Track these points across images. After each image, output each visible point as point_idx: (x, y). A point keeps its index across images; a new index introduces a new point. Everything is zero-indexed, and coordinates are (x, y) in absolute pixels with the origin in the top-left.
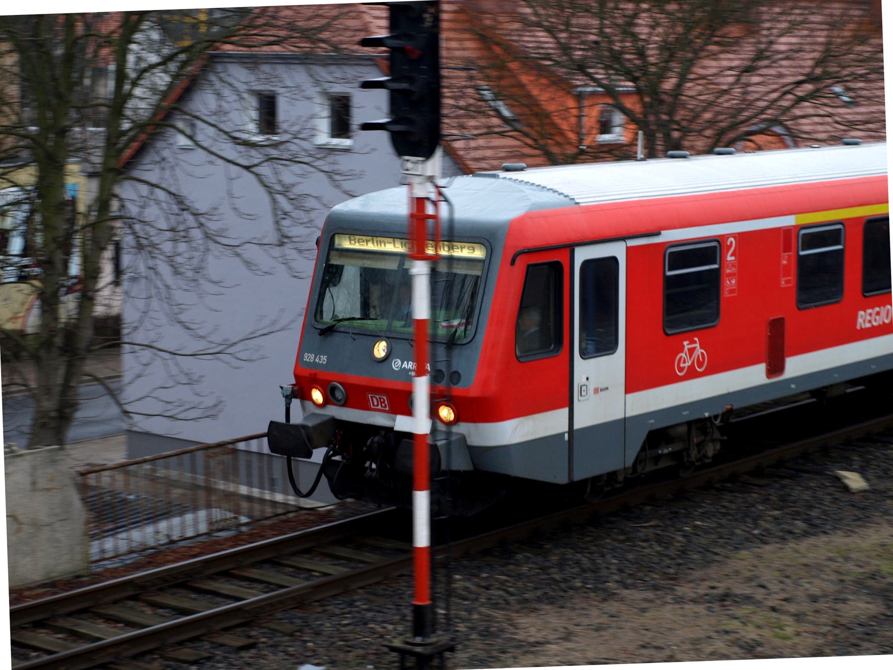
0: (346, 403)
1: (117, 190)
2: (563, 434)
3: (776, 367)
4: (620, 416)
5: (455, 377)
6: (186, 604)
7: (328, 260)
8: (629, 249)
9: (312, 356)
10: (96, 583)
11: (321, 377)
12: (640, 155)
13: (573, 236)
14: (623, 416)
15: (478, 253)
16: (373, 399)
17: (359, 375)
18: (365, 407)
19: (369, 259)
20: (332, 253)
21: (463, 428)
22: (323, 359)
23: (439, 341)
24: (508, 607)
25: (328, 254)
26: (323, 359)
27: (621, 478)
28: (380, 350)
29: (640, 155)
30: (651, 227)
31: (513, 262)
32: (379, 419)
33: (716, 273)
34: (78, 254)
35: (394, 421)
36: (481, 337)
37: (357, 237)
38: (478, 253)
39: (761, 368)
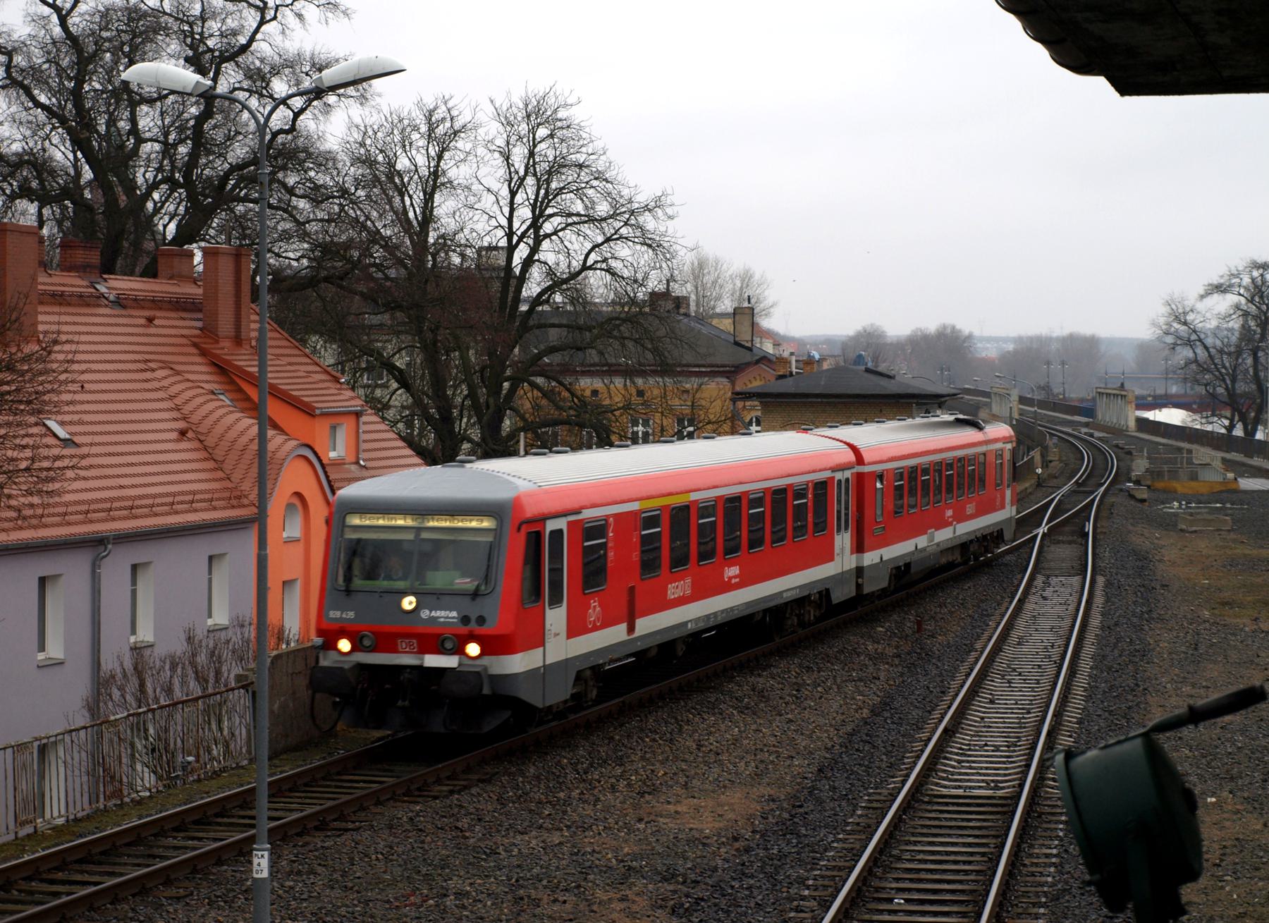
0: (374, 649)
2: (539, 668)
3: (631, 629)
4: (564, 657)
5: (481, 620)
8: (569, 523)
12: (522, 452)
13: (583, 504)
14: (541, 664)
15: (486, 523)
16: (402, 644)
18: (394, 650)
19: (376, 532)
20: (346, 529)
21: (487, 660)
22: (351, 615)
25: (342, 531)
26: (351, 615)
27: (555, 710)
28: (408, 603)
29: (522, 452)
30: (576, 506)
31: (519, 530)
32: (407, 660)
33: (604, 546)
34: (1182, 392)
35: (423, 659)
36: (499, 589)
37: (369, 515)
38: (486, 523)
39: (623, 627)
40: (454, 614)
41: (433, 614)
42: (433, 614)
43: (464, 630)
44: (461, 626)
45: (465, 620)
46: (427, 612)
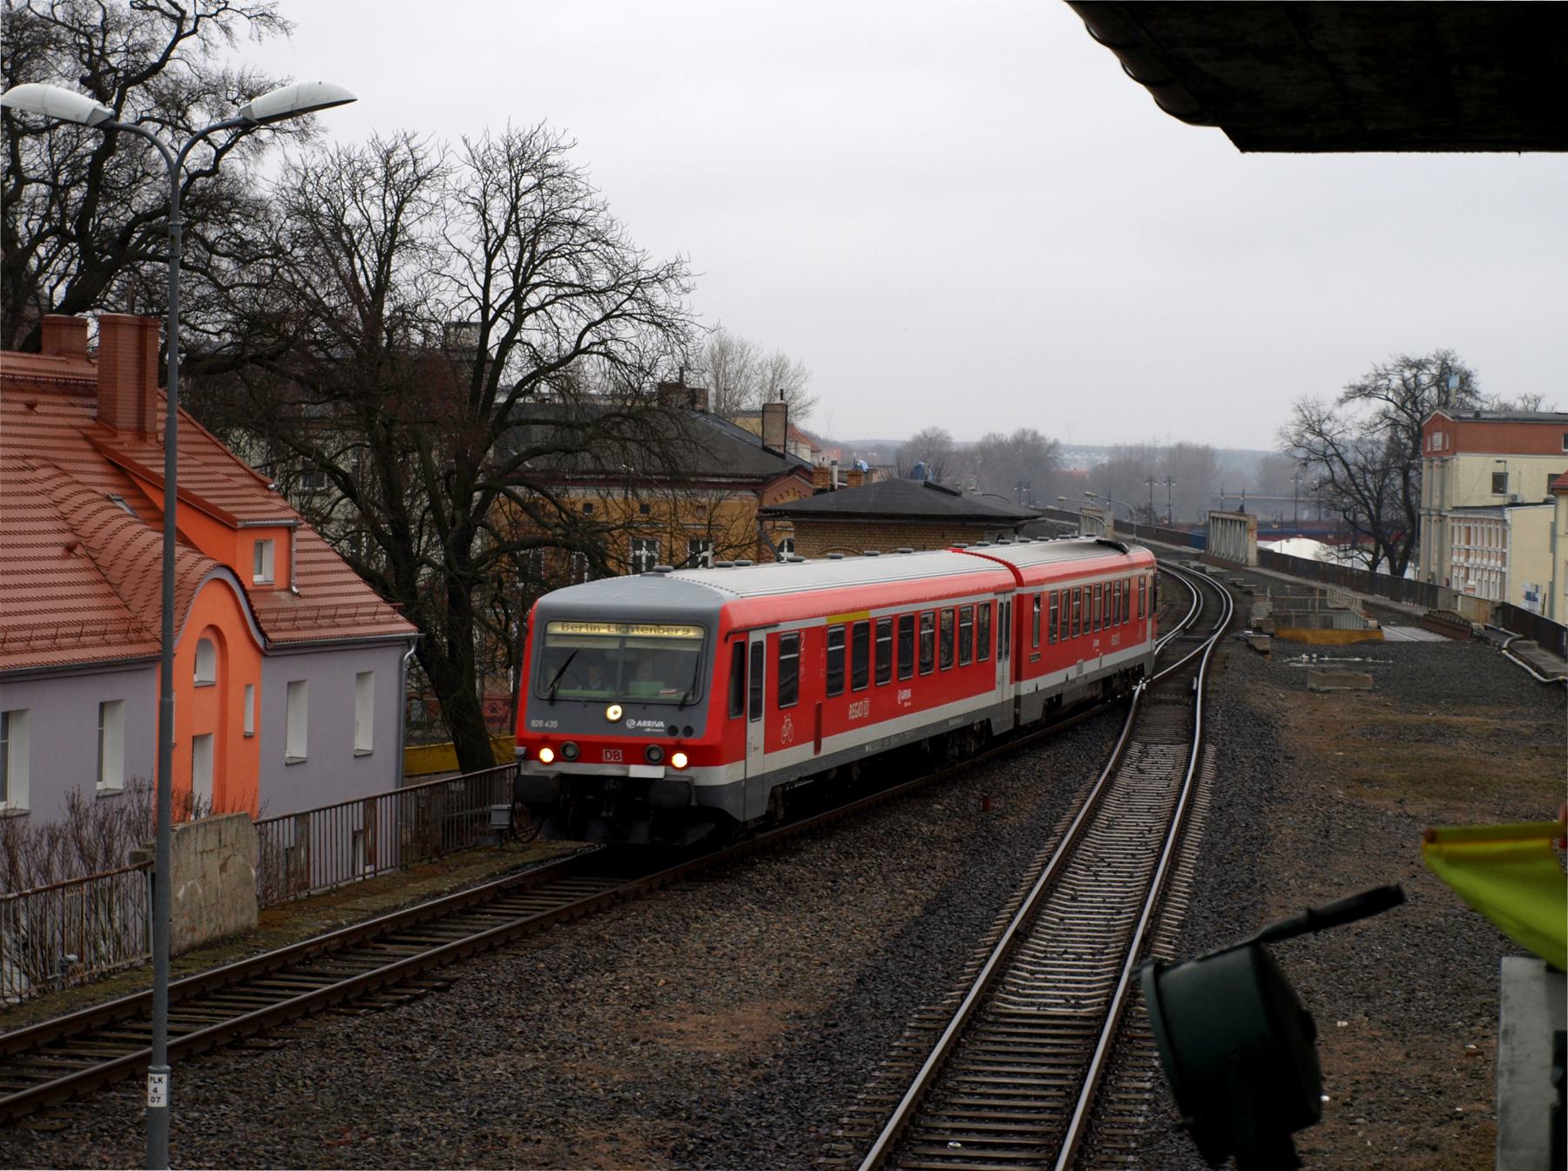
0: (577, 759)
1: (1365, 568)
5: (689, 731)
6: (107, 1053)
7: (544, 644)
9: (540, 723)
10: (1202, 702)
11: (552, 738)
14: (742, 778)
15: (693, 633)
16: (606, 754)
17: (593, 734)
18: (598, 760)
21: (693, 771)
22: (554, 724)
23: (149, 773)
24: (1145, 776)
26: (554, 724)
30: (770, 618)
36: (707, 699)
40: (661, 724)
41: (639, 724)
42: (639, 724)
43: (671, 740)
44: (667, 736)
45: (672, 730)
46: (634, 722)
